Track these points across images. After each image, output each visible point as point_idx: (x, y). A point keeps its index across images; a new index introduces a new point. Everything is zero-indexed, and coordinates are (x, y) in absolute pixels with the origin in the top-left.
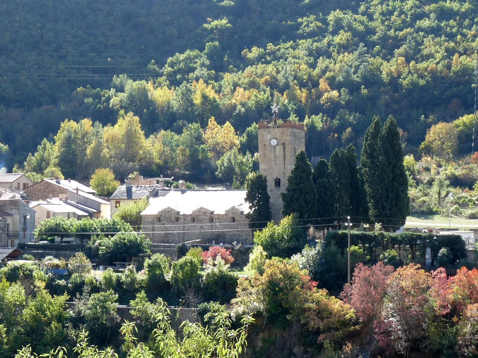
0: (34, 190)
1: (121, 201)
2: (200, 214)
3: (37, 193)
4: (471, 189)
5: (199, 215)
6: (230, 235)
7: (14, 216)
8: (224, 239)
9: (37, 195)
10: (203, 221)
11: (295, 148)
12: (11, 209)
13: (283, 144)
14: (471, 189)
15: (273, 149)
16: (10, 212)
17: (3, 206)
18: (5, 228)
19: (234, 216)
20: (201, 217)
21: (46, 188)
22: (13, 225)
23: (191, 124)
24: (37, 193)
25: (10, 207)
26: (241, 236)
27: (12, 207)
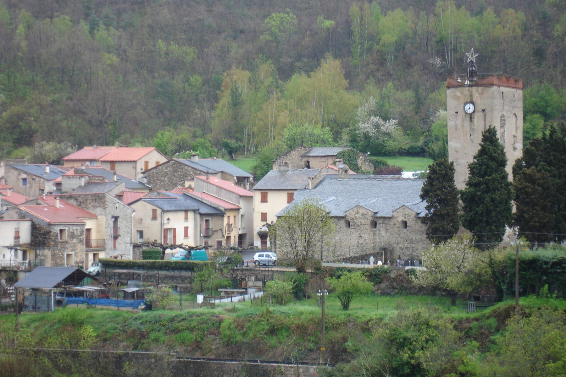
0: (157, 173)
1: (295, 192)
2: (358, 216)
3: (163, 178)
4: (262, 201)
5: (356, 217)
6: (401, 248)
7: (99, 217)
8: (391, 254)
9: (162, 181)
10: (362, 227)
11: (503, 116)
12: (95, 207)
13: (484, 110)
14: (262, 201)
15: (468, 118)
16: (93, 212)
17: (83, 202)
18: (82, 234)
19: (406, 220)
20: (360, 220)
21: (175, 171)
22: (98, 232)
23: (432, 59)
24: (163, 178)
25: (92, 204)
26: (417, 250)
27: (96, 204)
